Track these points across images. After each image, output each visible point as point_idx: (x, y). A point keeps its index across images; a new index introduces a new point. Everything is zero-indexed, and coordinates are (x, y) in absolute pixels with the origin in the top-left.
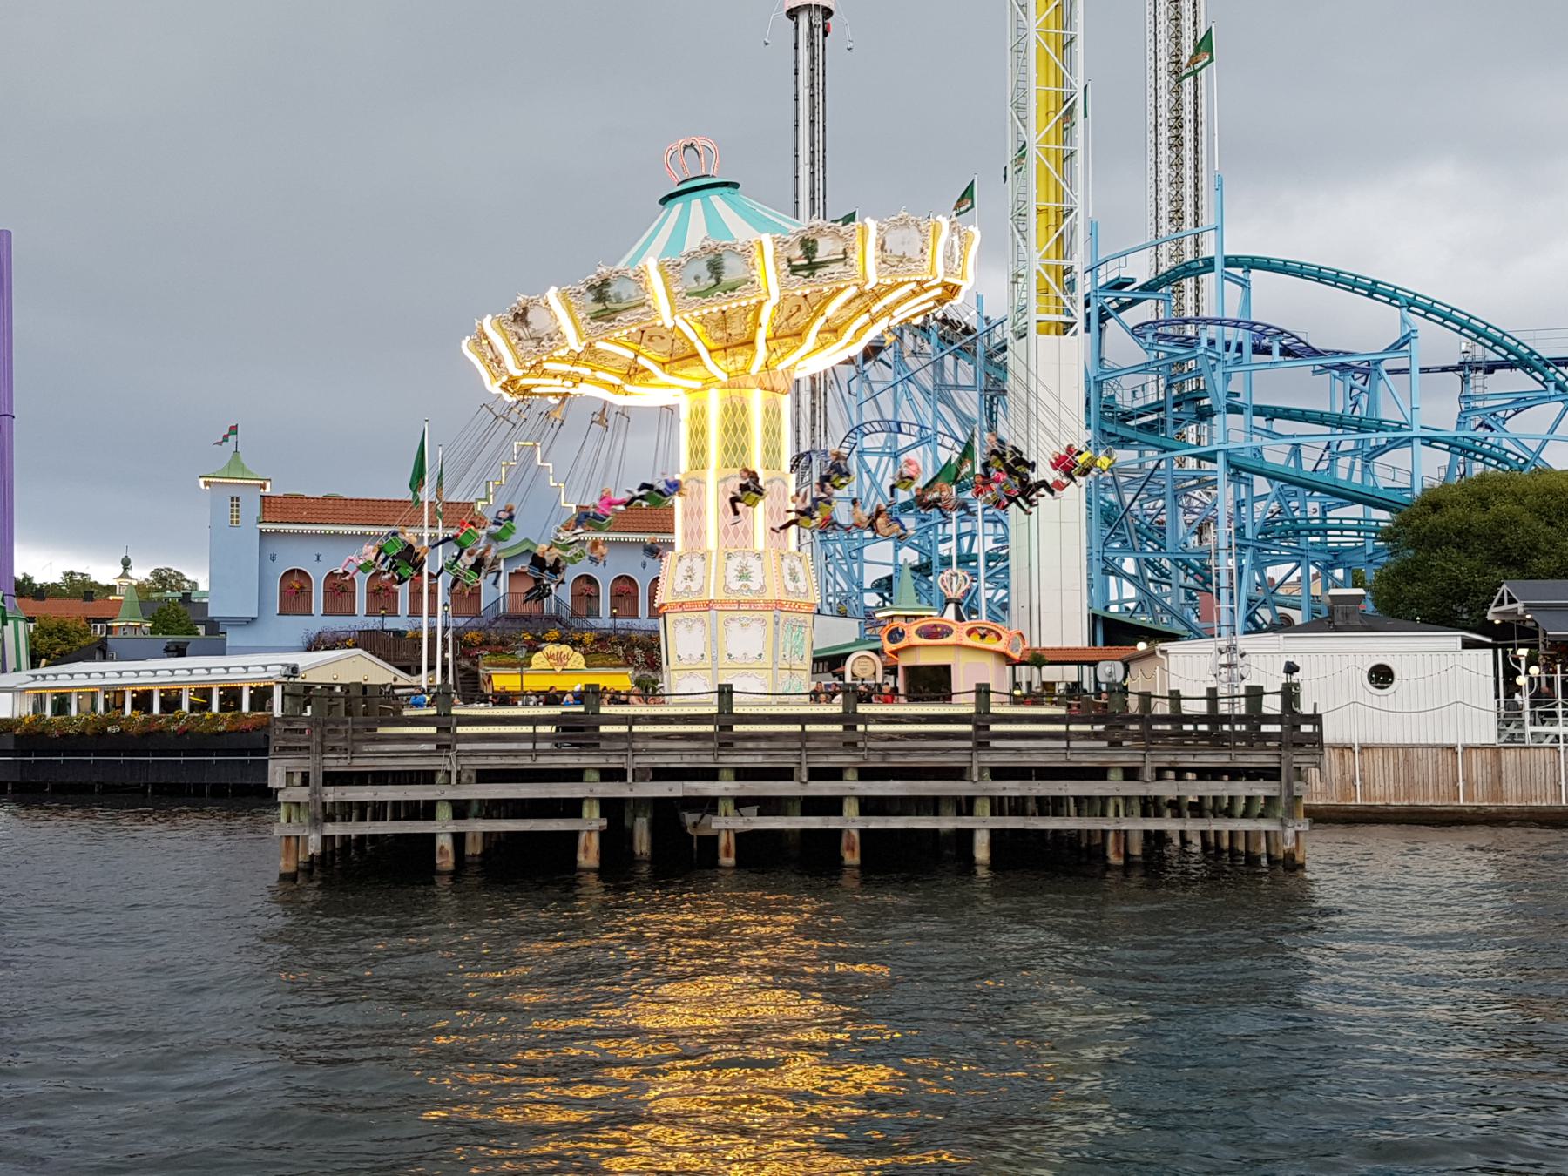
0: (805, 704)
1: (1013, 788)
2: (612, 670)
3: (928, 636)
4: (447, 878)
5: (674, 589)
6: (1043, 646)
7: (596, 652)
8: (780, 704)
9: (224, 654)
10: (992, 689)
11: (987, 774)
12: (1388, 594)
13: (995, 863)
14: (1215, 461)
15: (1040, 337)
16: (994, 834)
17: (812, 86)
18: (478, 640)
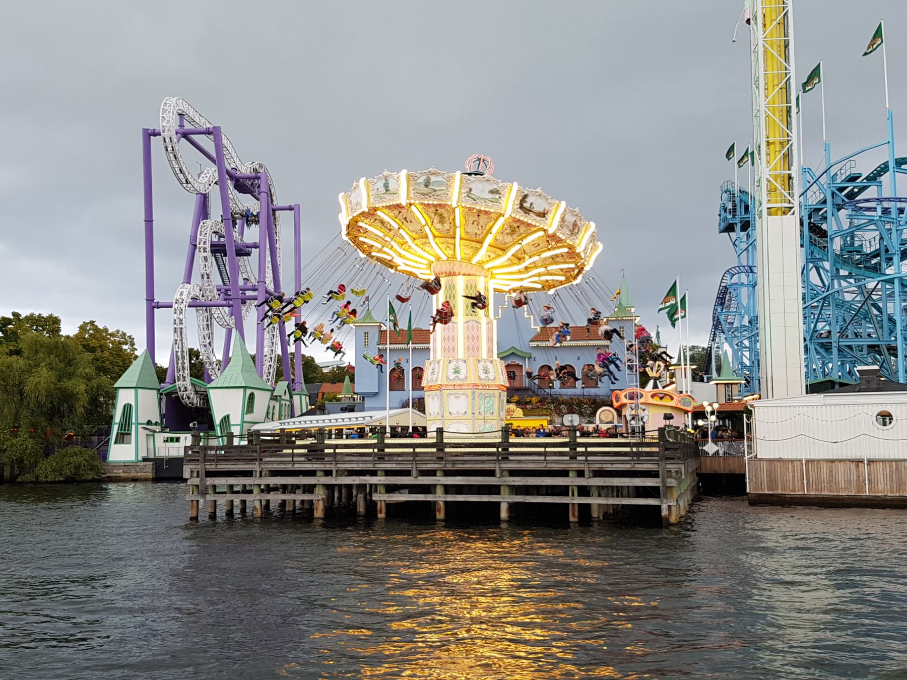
1: (518, 481)
2: (538, 418)
5: (447, 378)
7: (538, 408)
8: (476, 438)
9: (364, 411)
13: (511, 520)
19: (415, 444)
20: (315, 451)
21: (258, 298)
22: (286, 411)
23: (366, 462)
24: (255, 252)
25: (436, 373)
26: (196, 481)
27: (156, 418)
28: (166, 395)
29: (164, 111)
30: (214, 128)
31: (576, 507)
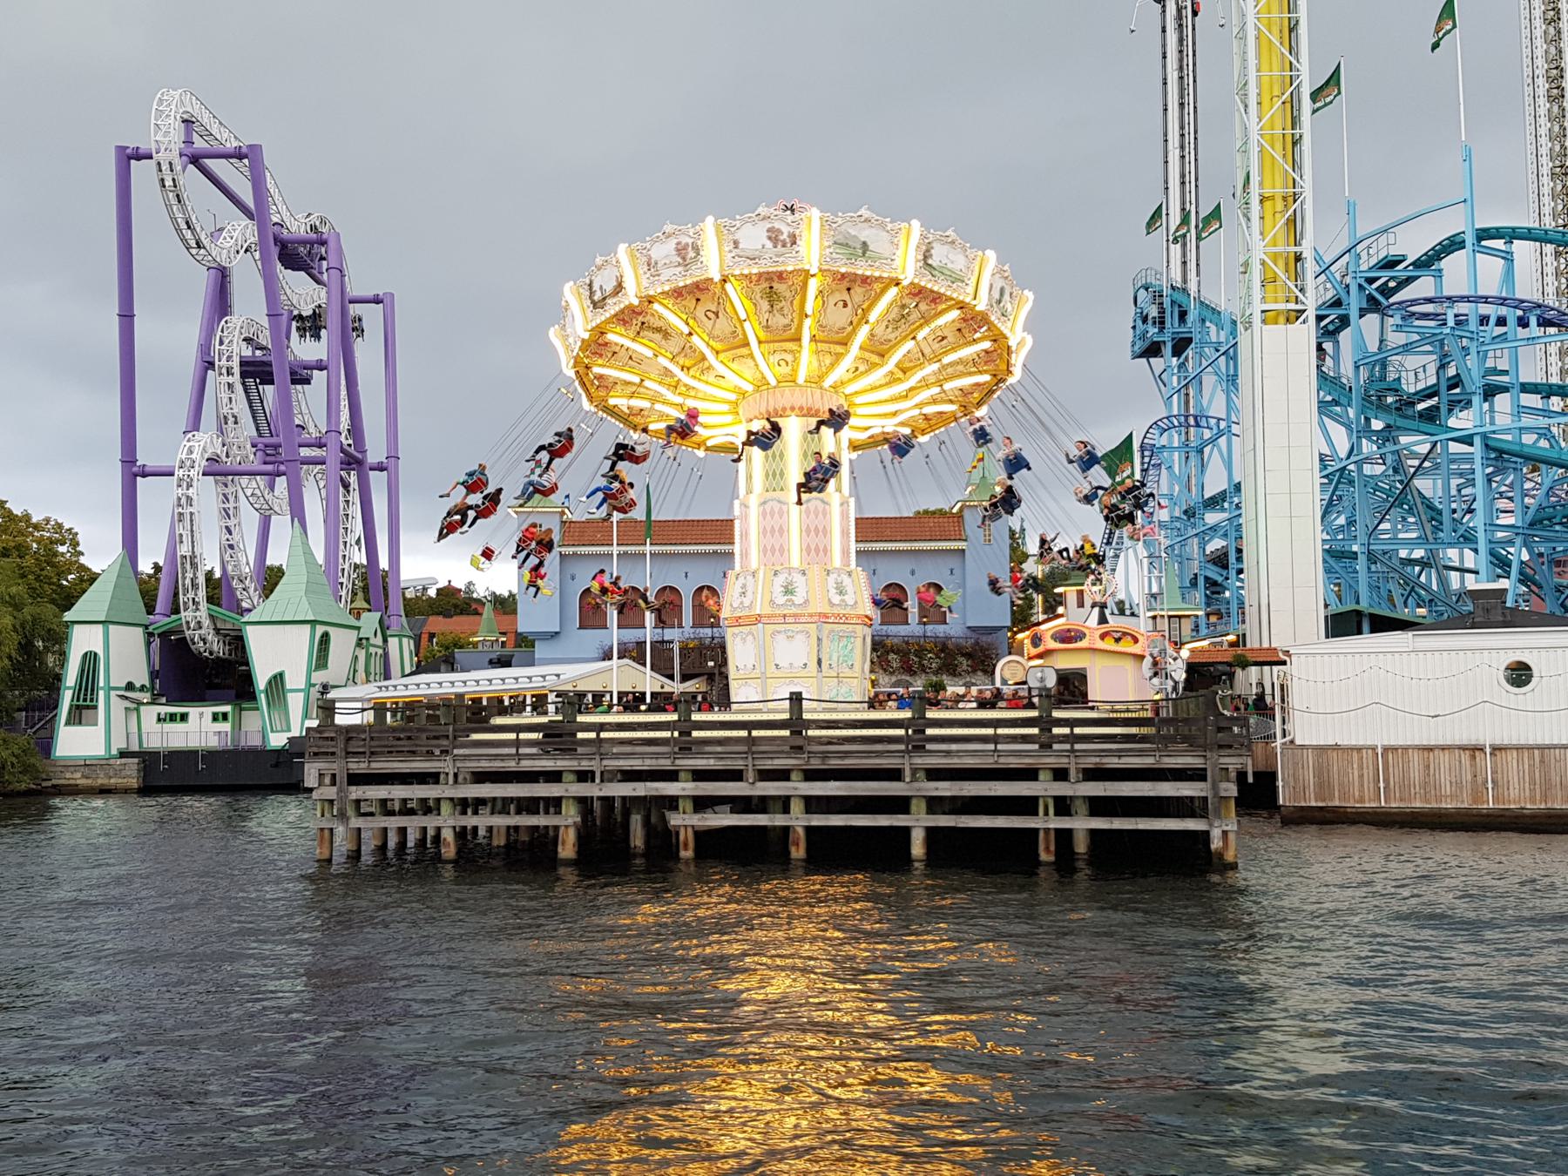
1: (945, 789)
3: (1063, 641)
4: (449, 866)
14: (1471, 444)
15: (1265, 327)
16: (931, 832)
17: (1181, 68)
19: (752, 722)
20: (560, 736)
21: (328, 462)
22: (376, 665)
23: (657, 756)
24: (319, 377)
25: (749, 594)
26: (331, 792)
27: (142, 678)
28: (159, 635)
29: (159, 112)
30: (250, 147)
31: (1052, 834)
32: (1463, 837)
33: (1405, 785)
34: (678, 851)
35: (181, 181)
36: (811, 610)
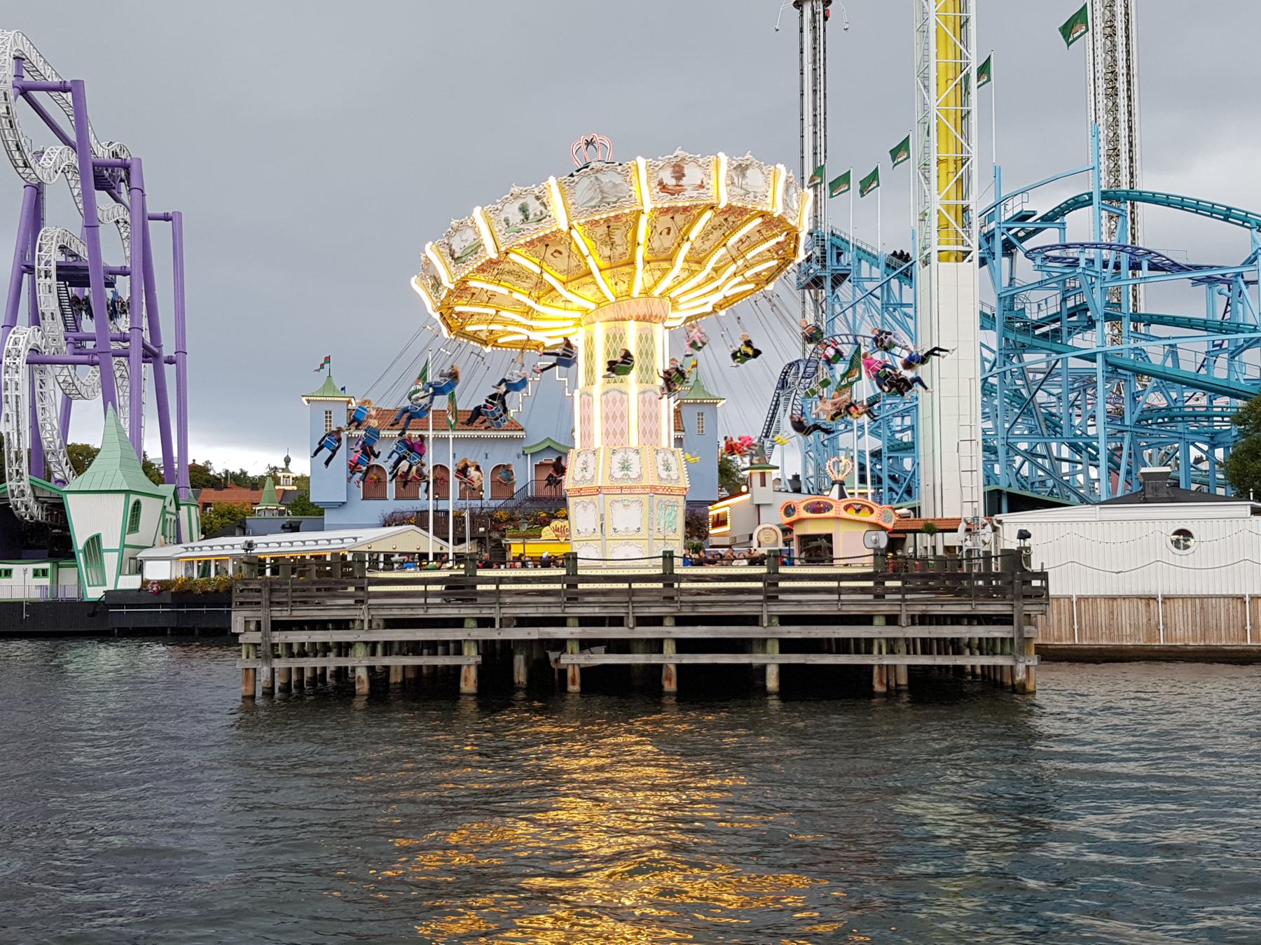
0: (743, 566)
1: (796, 632)
3: (814, 511)
5: (574, 478)
6: (945, 517)
9: (322, 530)
10: (675, 554)
11: (775, 620)
12: (1236, 469)
14: (1094, 361)
15: (941, 264)
16: (782, 667)
17: (814, 62)
18: (505, 517)
20: (462, 588)
23: (549, 605)
25: (590, 469)
26: (256, 637)
32: (1091, 667)
33: (1094, 627)
34: (566, 686)
35: (14, 109)
36: (644, 483)
